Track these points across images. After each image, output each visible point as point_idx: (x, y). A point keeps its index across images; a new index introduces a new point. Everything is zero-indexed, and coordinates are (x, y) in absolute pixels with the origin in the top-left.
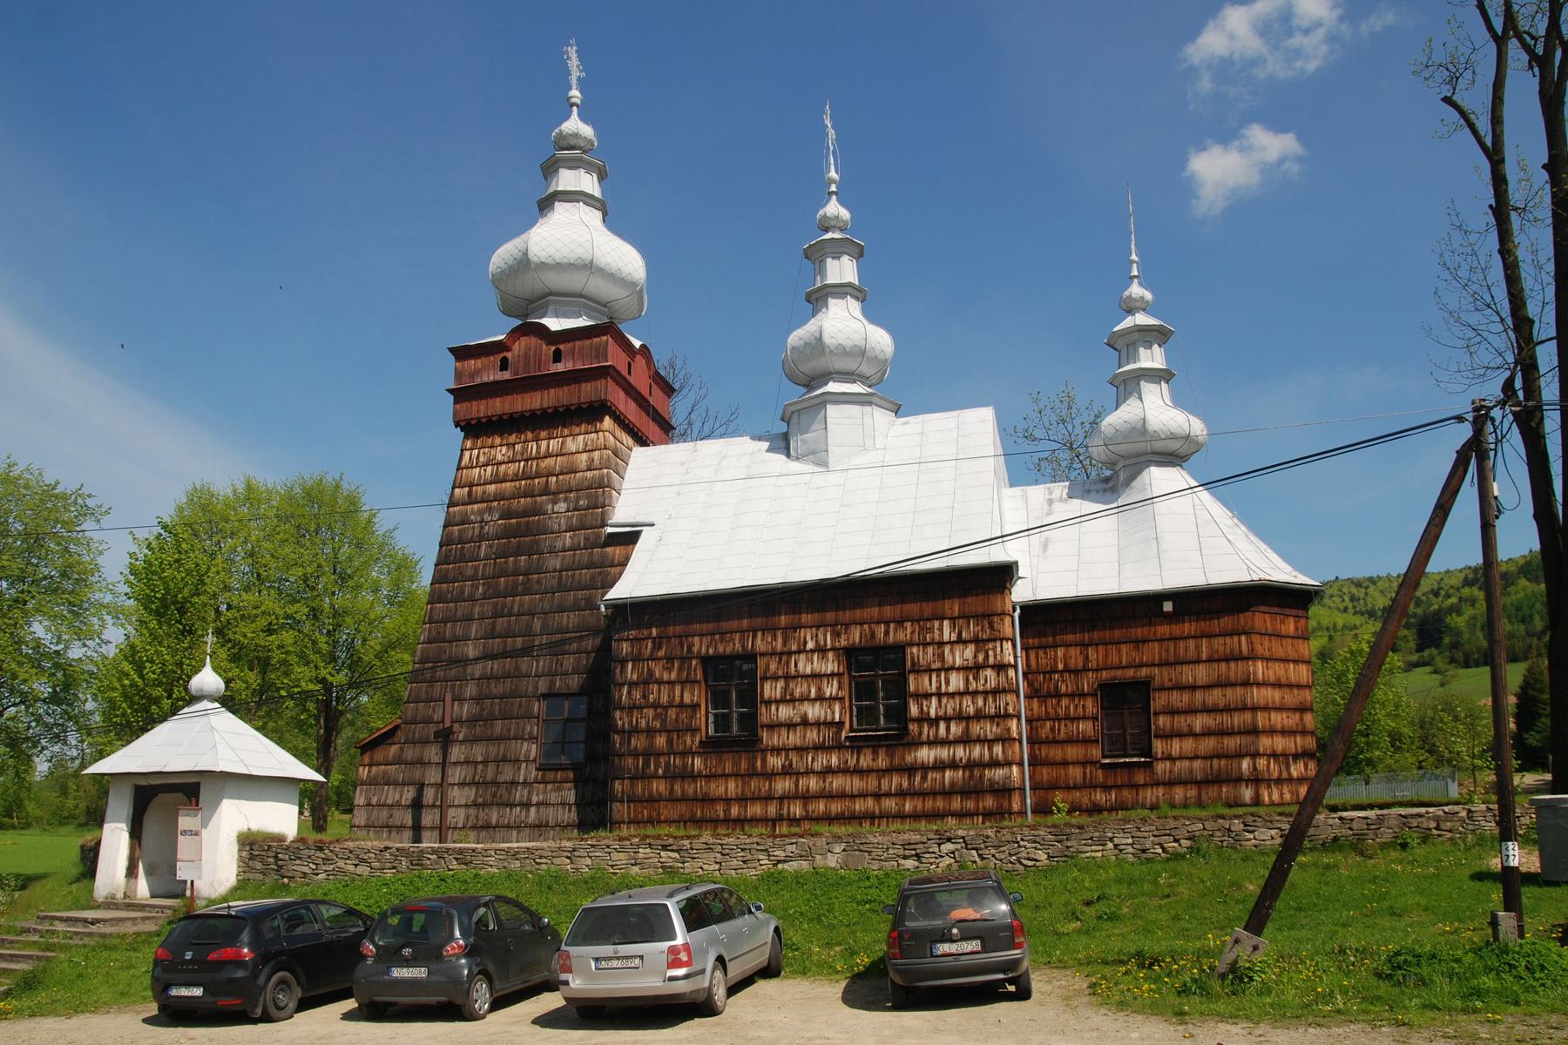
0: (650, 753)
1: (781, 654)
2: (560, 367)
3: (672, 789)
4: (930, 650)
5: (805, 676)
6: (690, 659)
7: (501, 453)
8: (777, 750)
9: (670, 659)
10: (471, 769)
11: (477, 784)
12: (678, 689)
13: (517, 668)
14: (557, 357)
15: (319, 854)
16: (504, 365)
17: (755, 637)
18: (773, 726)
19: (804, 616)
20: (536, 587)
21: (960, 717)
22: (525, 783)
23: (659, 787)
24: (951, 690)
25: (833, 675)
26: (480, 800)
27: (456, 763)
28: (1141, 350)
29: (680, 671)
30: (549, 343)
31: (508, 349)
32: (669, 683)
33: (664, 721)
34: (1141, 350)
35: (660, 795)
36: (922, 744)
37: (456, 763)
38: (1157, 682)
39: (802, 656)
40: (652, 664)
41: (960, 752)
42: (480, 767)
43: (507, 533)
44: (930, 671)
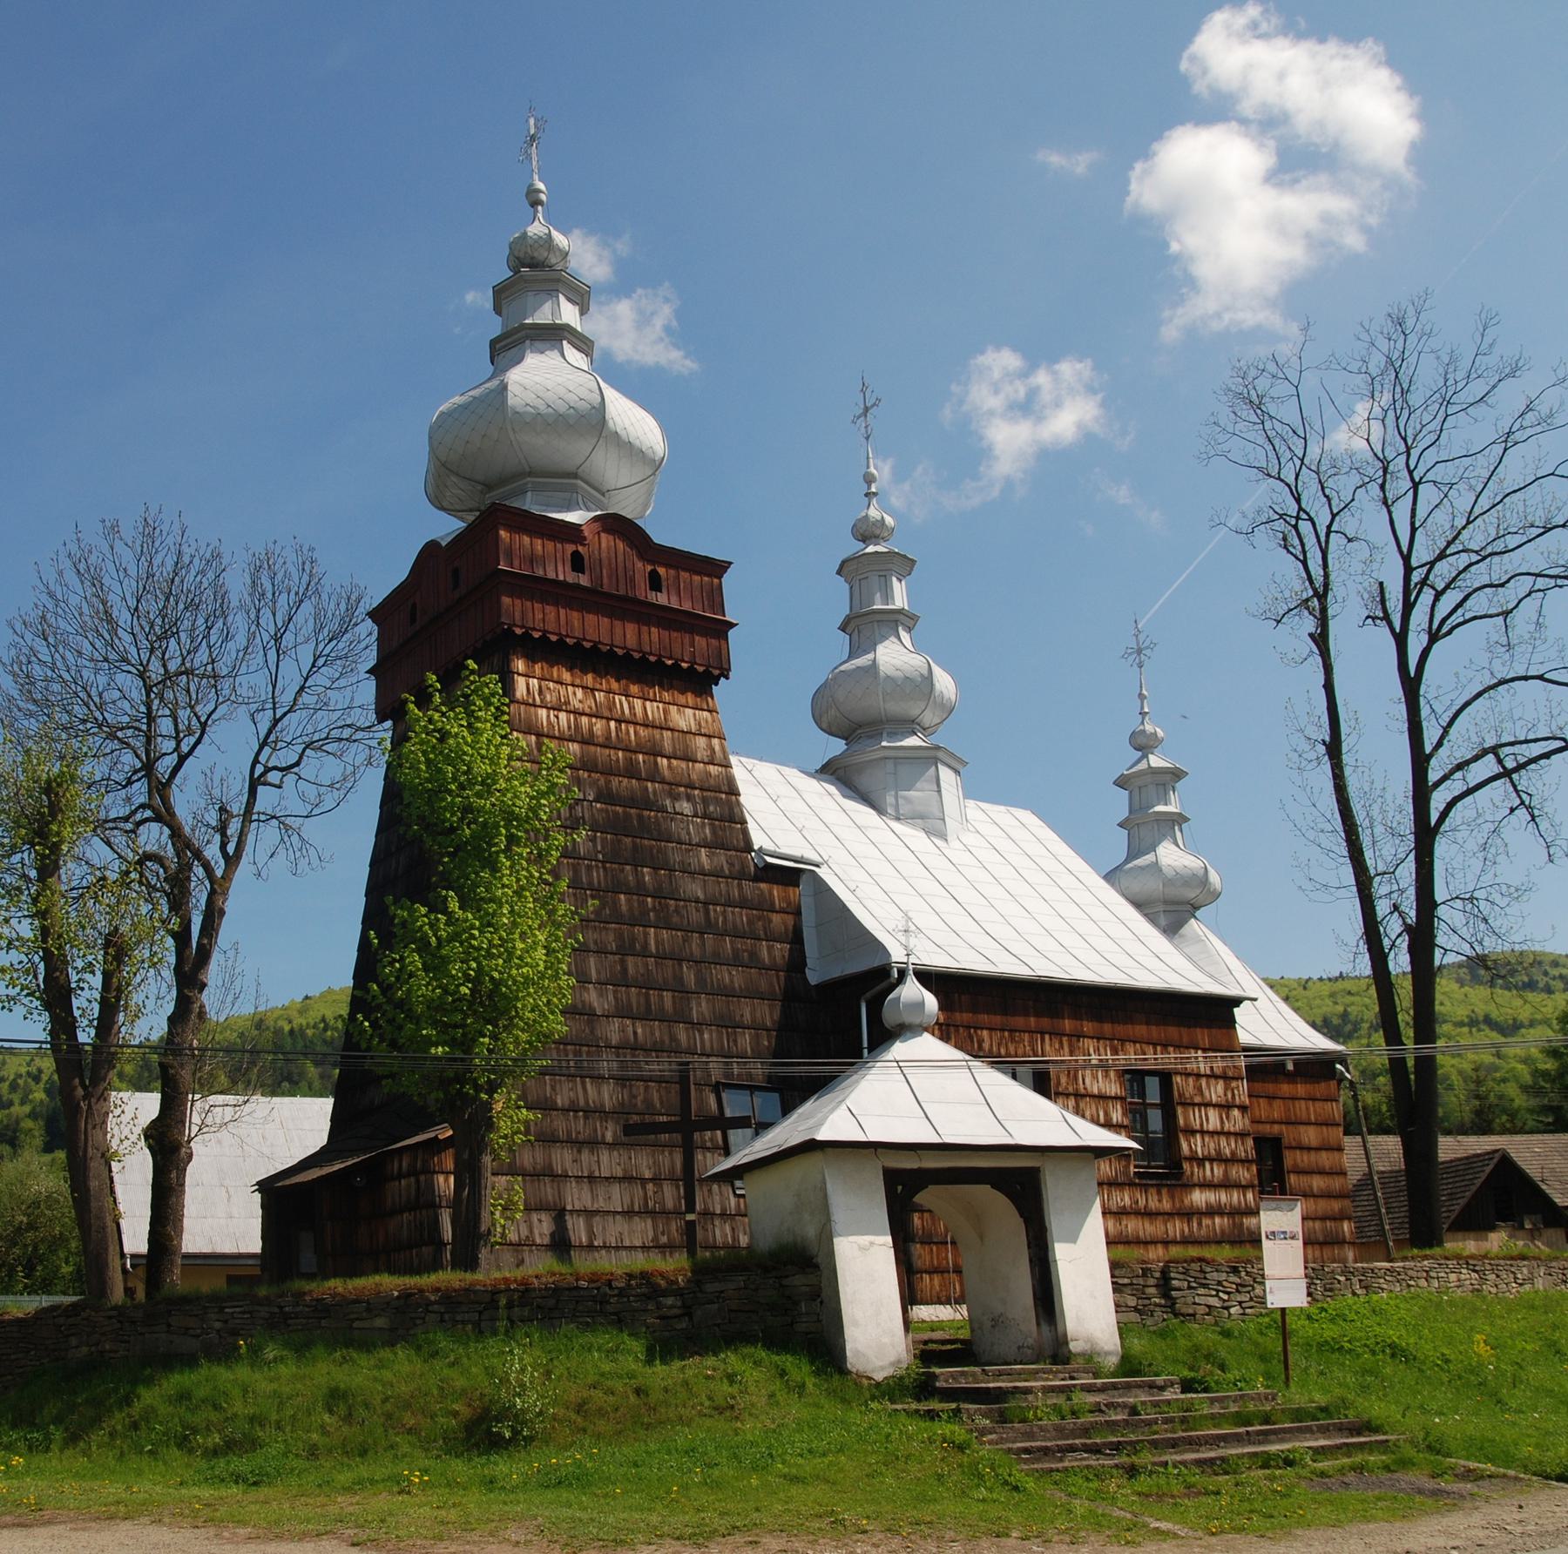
4: (1191, 1080)
5: (1093, 1096)
7: (577, 697)
10: (638, 1191)
11: (651, 1213)
13: (673, 1038)
14: (655, 583)
15: (1233, 1278)
19: (1138, 1027)
20: (675, 919)
21: (1219, 1159)
22: (723, 1215)
24: (1211, 1128)
25: (1116, 1098)
26: (664, 1239)
30: (642, 557)
36: (1195, 1185)
38: (1285, 1142)
41: (1223, 1197)
42: (650, 1186)
44: (1194, 1105)
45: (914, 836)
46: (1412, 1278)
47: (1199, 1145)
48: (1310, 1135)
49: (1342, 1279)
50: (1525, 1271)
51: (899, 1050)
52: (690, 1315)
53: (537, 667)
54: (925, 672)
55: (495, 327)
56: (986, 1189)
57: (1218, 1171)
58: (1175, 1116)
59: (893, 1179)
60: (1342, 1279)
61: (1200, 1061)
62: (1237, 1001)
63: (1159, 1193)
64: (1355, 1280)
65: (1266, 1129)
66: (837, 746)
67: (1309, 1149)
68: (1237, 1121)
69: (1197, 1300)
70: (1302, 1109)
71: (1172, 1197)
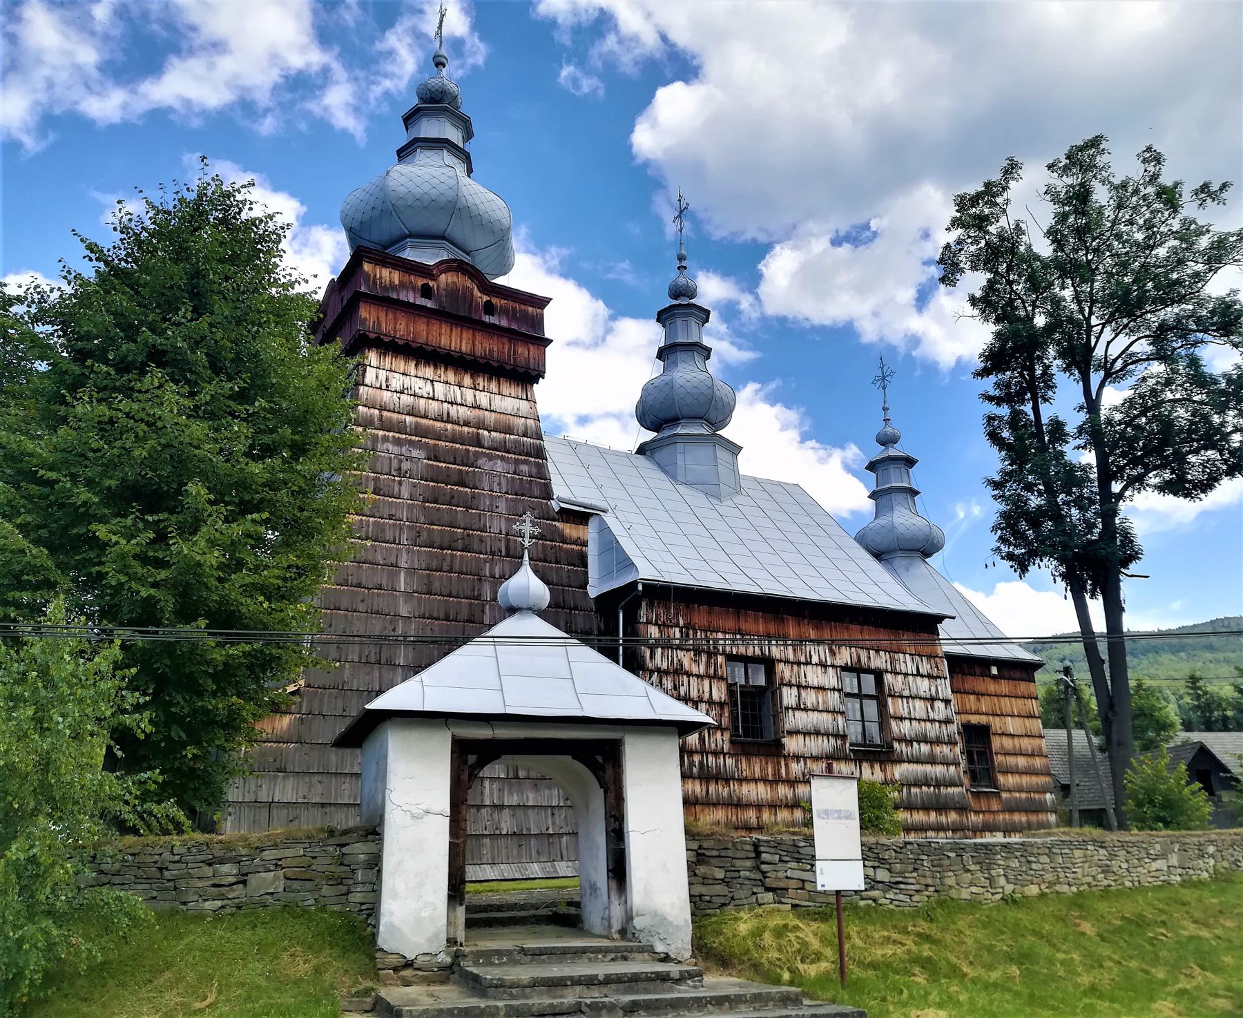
1: (792, 663)
2: (487, 319)
3: (707, 792)
6: (716, 654)
8: (797, 757)
9: (698, 651)
12: (706, 682)
14: (489, 308)
16: (426, 292)
18: (794, 733)
21: (923, 739)
25: (834, 689)
27: (1069, 737)
29: (708, 665)
31: (434, 278)
32: (698, 676)
35: (697, 798)
37: (1069, 737)
39: (809, 667)
43: (434, 476)
44: (902, 697)
45: (696, 498)
46: (1032, 854)
47: (906, 728)
48: (1012, 725)
49: (952, 855)
50: (1158, 847)
51: (507, 627)
52: (244, 882)
53: (388, 359)
54: (710, 384)
55: (403, 139)
56: (567, 759)
57: (925, 748)
58: (886, 705)
59: (460, 748)
60: (952, 855)
61: (906, 663)
62: (940, 618)
63: (872, 767)
64: (966, 856)
65: (974, 719)
66: (650, 435)
67: (1013, 736)
68: (940, 710)
69: (789, 874)
70: (1006, 704)
71: (883, 770)
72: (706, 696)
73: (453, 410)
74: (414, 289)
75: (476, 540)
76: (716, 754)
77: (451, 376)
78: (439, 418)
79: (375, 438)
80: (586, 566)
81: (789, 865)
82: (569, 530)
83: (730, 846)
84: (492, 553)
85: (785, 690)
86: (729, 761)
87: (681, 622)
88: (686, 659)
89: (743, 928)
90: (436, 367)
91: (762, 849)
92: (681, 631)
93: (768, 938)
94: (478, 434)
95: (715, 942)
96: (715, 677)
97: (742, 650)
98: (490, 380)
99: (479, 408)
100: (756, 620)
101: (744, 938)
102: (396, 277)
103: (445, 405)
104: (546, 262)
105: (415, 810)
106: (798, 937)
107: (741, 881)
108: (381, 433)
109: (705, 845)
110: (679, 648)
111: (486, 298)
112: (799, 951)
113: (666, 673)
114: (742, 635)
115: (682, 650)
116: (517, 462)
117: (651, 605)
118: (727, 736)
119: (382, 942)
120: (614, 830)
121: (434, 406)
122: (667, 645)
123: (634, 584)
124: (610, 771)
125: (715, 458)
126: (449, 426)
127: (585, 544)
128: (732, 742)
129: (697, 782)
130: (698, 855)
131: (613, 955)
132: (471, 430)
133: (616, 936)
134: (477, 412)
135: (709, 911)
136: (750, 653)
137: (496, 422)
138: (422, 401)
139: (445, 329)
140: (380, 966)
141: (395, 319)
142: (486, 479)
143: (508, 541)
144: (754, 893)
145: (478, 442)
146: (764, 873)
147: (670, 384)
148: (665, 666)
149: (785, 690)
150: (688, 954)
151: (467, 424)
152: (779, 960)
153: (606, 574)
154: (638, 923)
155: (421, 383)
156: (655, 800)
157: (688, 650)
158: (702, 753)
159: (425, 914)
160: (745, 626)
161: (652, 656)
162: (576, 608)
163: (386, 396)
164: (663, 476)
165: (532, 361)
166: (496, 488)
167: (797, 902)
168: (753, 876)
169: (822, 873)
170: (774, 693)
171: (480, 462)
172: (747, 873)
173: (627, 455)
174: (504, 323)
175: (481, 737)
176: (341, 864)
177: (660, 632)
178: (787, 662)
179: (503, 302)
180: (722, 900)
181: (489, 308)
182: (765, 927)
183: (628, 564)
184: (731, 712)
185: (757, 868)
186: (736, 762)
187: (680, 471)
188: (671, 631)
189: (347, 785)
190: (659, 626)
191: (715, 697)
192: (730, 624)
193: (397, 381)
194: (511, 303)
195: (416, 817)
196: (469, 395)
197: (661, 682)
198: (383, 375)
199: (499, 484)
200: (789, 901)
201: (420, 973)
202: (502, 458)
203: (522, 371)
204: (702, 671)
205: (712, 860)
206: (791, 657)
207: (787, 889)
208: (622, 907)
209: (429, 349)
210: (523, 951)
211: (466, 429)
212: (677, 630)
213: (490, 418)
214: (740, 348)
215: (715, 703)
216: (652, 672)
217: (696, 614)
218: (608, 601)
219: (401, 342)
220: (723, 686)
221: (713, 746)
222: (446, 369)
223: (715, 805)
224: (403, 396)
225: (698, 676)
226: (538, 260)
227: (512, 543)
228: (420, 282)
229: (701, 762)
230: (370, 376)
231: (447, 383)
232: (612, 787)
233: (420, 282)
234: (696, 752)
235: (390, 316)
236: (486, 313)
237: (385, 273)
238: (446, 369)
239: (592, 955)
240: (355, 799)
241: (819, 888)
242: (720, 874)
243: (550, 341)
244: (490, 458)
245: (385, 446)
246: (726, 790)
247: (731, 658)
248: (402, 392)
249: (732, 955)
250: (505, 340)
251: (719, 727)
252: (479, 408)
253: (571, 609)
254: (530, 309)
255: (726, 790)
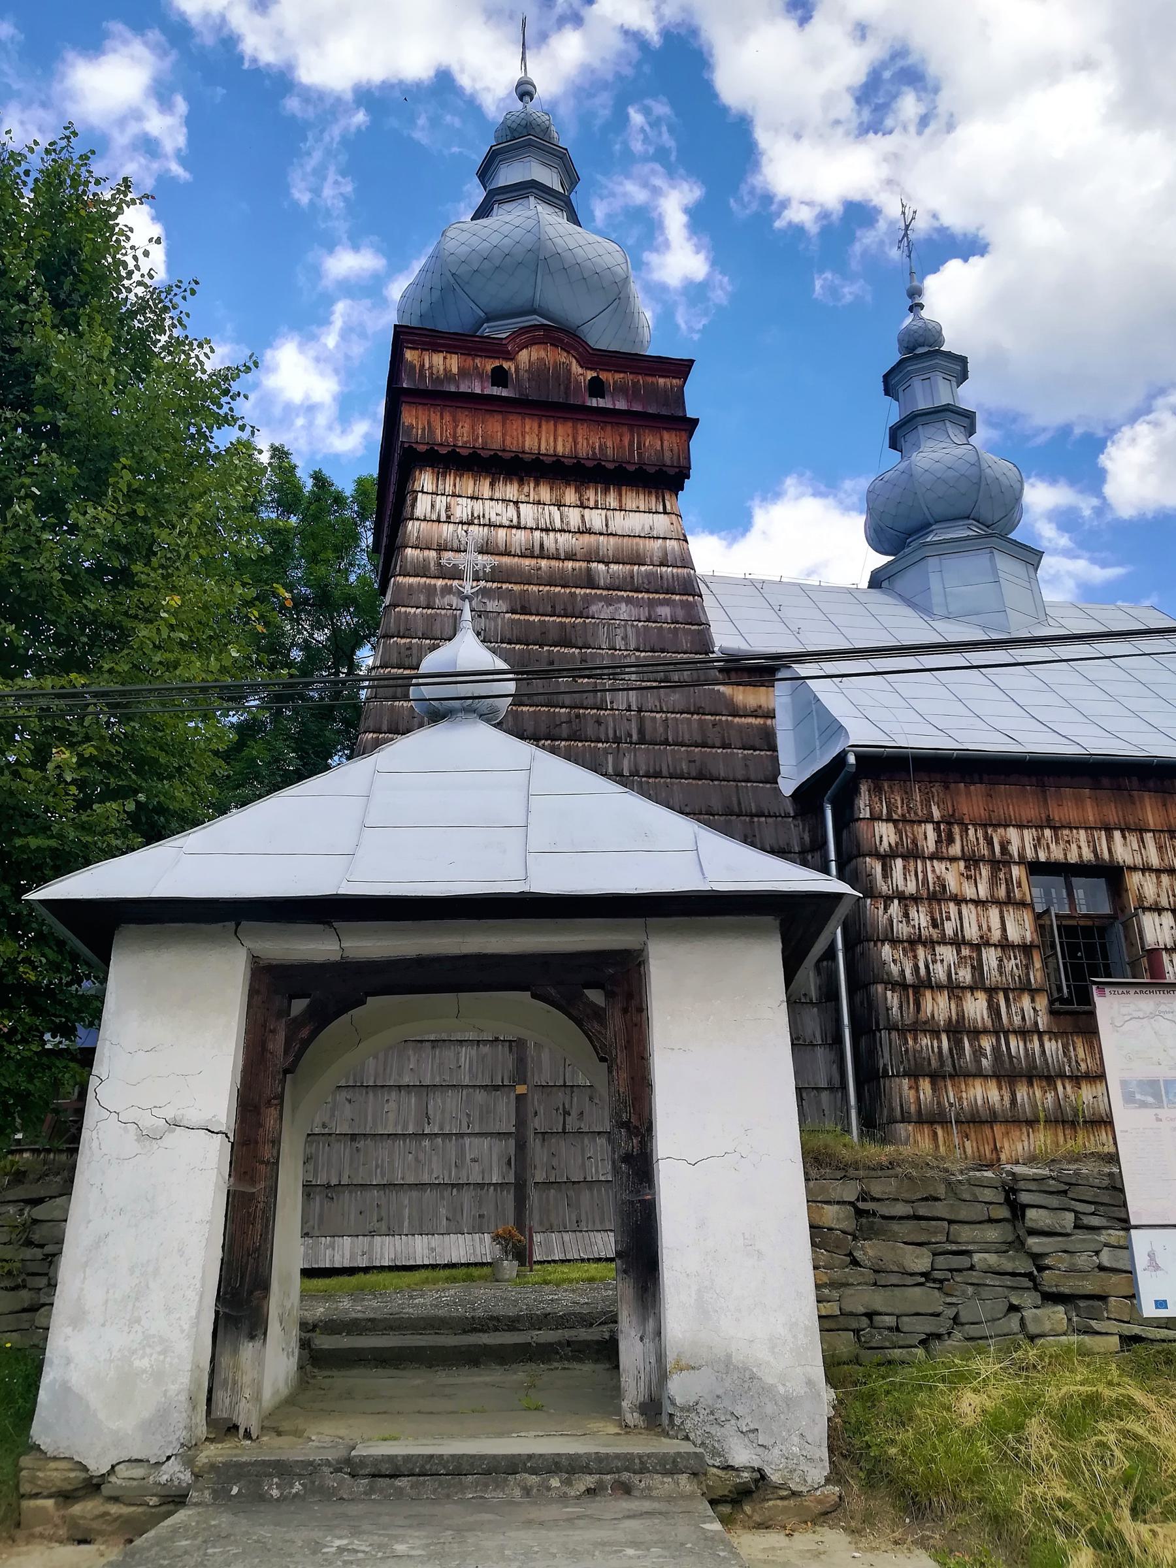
0: (957, 1029)
1: (1158, 872)
2: (594, 402)
3: (1013, 1101)
9: (972, 861)
14: (597, 388)
16: (500, 377)
17: (1110, 839)
23: (984, 1094)
28: (725, 303)
29: (993, 881)
31: (510, 357)
32: (977, 902)
33: (978, 969)
34: (725, 303)
35: (993, 1112)
40: (940, 867)
53: (449, 481)
54: (973, 460)
59: (271, 985)
72: (996, 935)
73: (549, 540)
74: (481, 376)
75: (591, 723)
76: (1023, 1033)
77: (545, 493)
78: (528, 553)
79: (431, 591)
80: (774, 749)
81: (1103, 1237)
82: (744, 696)
83: (941, 1191)
84: (617, 740)
85: (1148, 921)
86: (1051, 1046)
87: (937, 814)
88: (952, 876)
89: (970, 1405)
90: (521, 483)
91: (1025, 1198)
92: (937, 830)
93: (1039, 1436)
94: (589, 570)
95: (895, 1443)
96: (1010, 901)
97: (1057, 854)
98: (606, 491)
99: (589, 532)
100: (1079, 801)
101: (969, 1435)
102: (454, 363)
103: (537, 534)
104: (841, 503)
105: (148, 1121)
106: (1126, 1433)
107: (974, 1276)
108: (440, 583)
109: (876, 1190)
110: (936, 856)
111: (590, 375)
112: (1127, 1481)
113: (916, 899)
114: (1055, 829)
115: (941, 859)
116: (652, 604)
117: (877, 790)
118: (1042, 1002)
119: (40, 1433)
120: (627, 1158)
121: (520, 537)
122: (912, 854)
123: (841, 758)
124: (616, 1021)
125: (995, 570)
126: (544, 563)
127: (771, 715)
128: (1052, 1012)
129: (992, 1086)
130: (859, 1213)
131: (590, 1481)
132: (577, 565)
133: (633, 1418)
134: (586, 539)
135: (897, 1353)
136: (1073, 858)
137: (616, 549)
138: (502, 533)
139: (530, 425)
140: (25, 1488)
141: (455, 421)
142: (602, 633)
143: (641, 721)
144: (1013, 1308)
145: (590, 581)
146: (1036, 1257)
147: (909, 473)
148: (911, 888)
149: (1148, 921)
150: (817, 1473)
151: (571, 556)
152: (1064, 1505)
153: (805, 752)
154: (679, 1388)
155: (499, 507)
156: (724, 1080)
157: (953, 859)
158: (996, 1033)
159: (141, 1363)
160: (1057, 815)
161: (887, 873)
162: (761, 814)
163: (447, 530)
164: (909, 611)
165: (667, 454)
166: (619, 643)
167: (1136, 1330)
168: (1009, 1266)
169: (1154, 1266)
170: (1127, 926)
171: (593, 609)
172: (992, 1259)
173: (851, 592)
174: (621, 405)
175: (319, 958)
176: (29, 1243)
177: (899, 832)
178: (1146, 869)
179: (618, 376)
180: (926, 1326)
181: (597, 388)
182: (1034, 1402)
183: (839, 729)
184: (1045, 964)
185: (1018, 1244)
186: (1065, 1047)
187: (937, 599)
188: (919, 830)
189: (392, 1105)
190: (895, 822)
191: (1014, 935)
192: (1030, 811)
193: (462, 508)
194: (631, 377)
195: (147, 1136)
196: (574, 517)
197: (906, 915)
198: (441, 502)
199: (625, 638)
200: (1113, 1327)
201: (114, 1509)
202: (629, 601)
203: (652, 470)
204: (983, 892)
205: (895, 1226)
206: (1155, 861)
207: (1103, 1298)
208: (650, 1345)
209: (507, 456)
210: (351, 1467)
211: (569, 565)
212: (930, 828)
213: (607, 544)
214: (1104, 565)
215: (1013, 946)
216: (888, 900)
217: (963, 799)
218: (809, 796)
219: (465, 452)
220: (1027, 917)
221: (1017, 1020)
222: (537, 485)
223: (1031, 1123)
224: (471, 528)
225: (977, 902)
226: (830, 501)
227: (648, 725)
228: (490, 365)
229: (996, 1050)
230: (423, 505)
231: (539, 503)
232: (621, 1057)
233: (490, 365)
234: (985, 1031)
235: (447, 417)
236: (592, 395)
237: (438, 360)
238: (537, 485)
239: (533, 1479)
240: (405, 1127)
241: (1149, 1310)
242: (920, 1261)
243: (694, 422)
244: (609, 601)
245: (447, 600)
246: (1050, 1096)
247: (1036, 868)
248: (470, 523)
249: (934, 1484)
250: (625, 429)
251: (1026, 988)
252: (589, 532)
253: (752, 815)
254: (661, 381)
255: (1050, 1096)
